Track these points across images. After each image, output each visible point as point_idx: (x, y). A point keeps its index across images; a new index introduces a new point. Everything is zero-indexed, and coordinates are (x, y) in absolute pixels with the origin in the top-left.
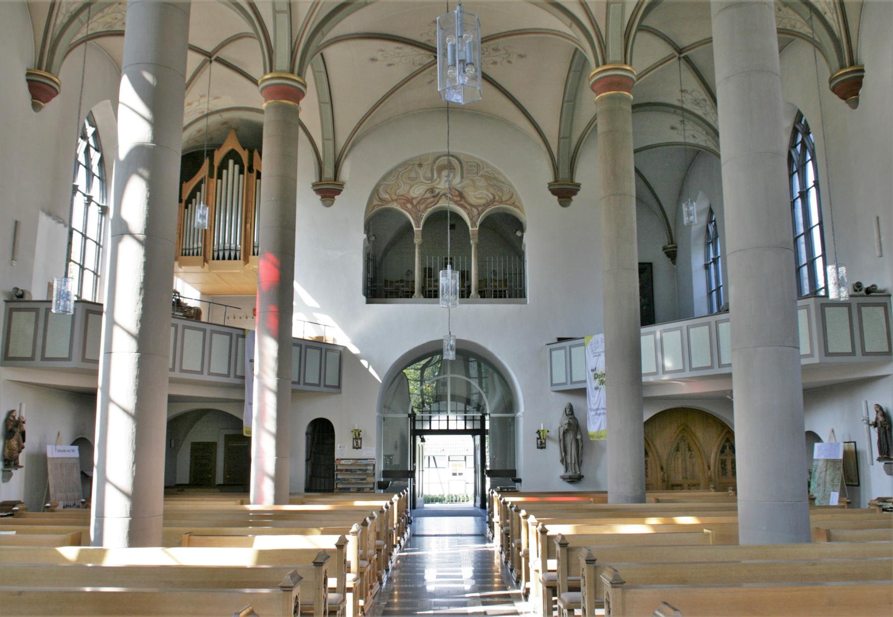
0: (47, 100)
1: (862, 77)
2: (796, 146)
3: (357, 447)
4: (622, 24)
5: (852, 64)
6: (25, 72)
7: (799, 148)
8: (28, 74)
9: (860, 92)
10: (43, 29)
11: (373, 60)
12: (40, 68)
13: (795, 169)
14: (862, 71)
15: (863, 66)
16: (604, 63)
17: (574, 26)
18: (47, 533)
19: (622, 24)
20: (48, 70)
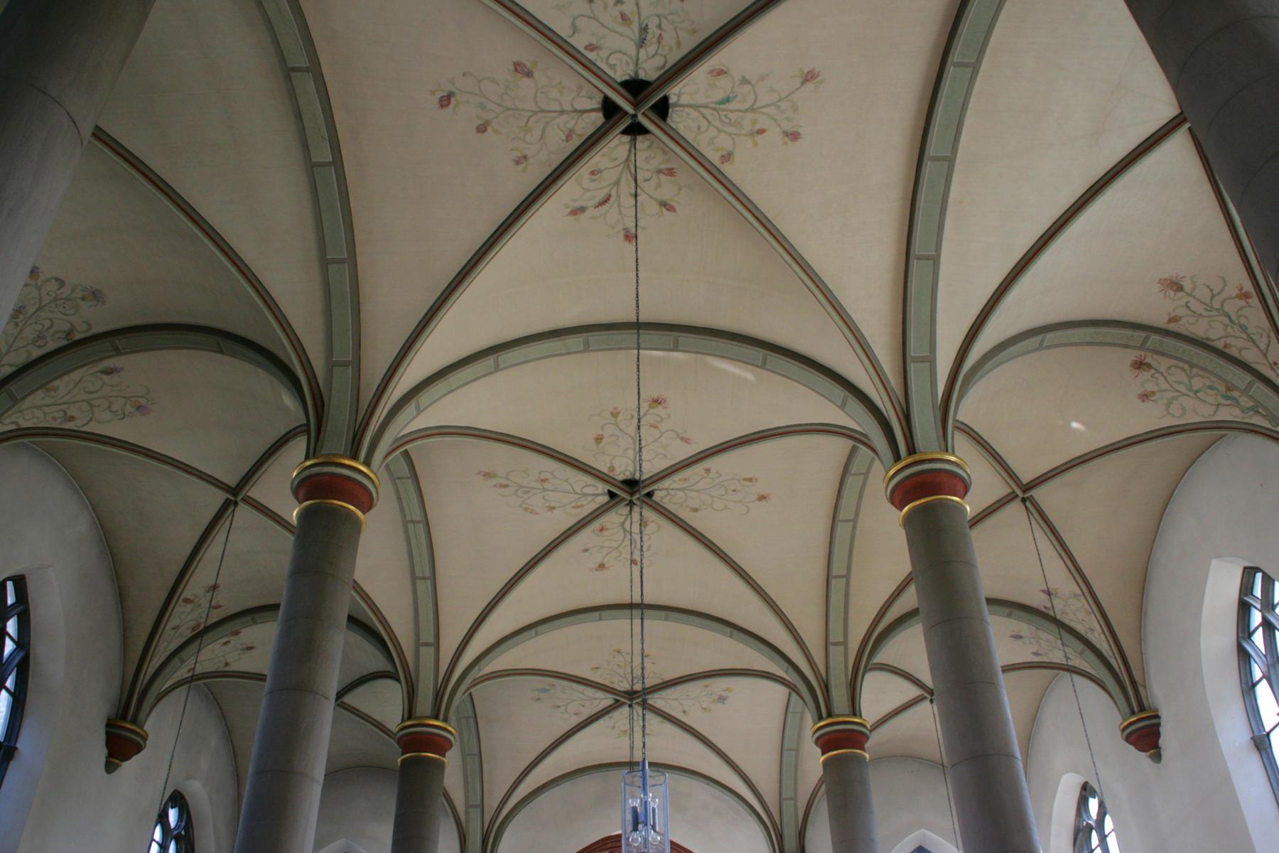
0: (127, 758)
1: (1159, 725)
2: (1250, 634)
3: (1004, 671)
4: (846, 668)
5: (1142, 708)
6: (105, 722)
7: (1258, 638)
8: (108, 725)
9: (1161, 741)
10: (140, 650)
11: (602, 566)
12: (124, 718)
13: (1257, 673)
14: (1157, 717)
15: (1157, 710)
16: (830, 715)
17: (791, 670)
18: (113, 445)
19: (846, 668)
20: (134, 721)
